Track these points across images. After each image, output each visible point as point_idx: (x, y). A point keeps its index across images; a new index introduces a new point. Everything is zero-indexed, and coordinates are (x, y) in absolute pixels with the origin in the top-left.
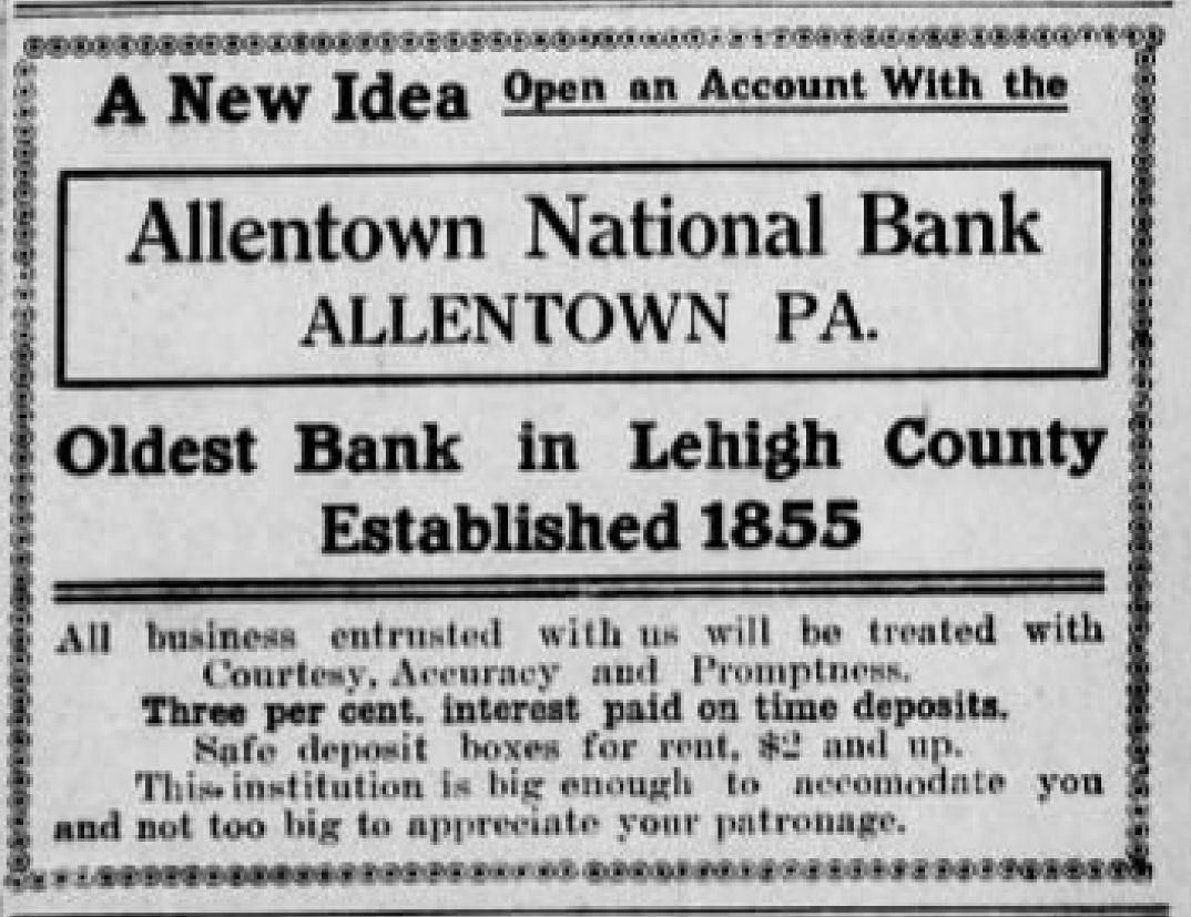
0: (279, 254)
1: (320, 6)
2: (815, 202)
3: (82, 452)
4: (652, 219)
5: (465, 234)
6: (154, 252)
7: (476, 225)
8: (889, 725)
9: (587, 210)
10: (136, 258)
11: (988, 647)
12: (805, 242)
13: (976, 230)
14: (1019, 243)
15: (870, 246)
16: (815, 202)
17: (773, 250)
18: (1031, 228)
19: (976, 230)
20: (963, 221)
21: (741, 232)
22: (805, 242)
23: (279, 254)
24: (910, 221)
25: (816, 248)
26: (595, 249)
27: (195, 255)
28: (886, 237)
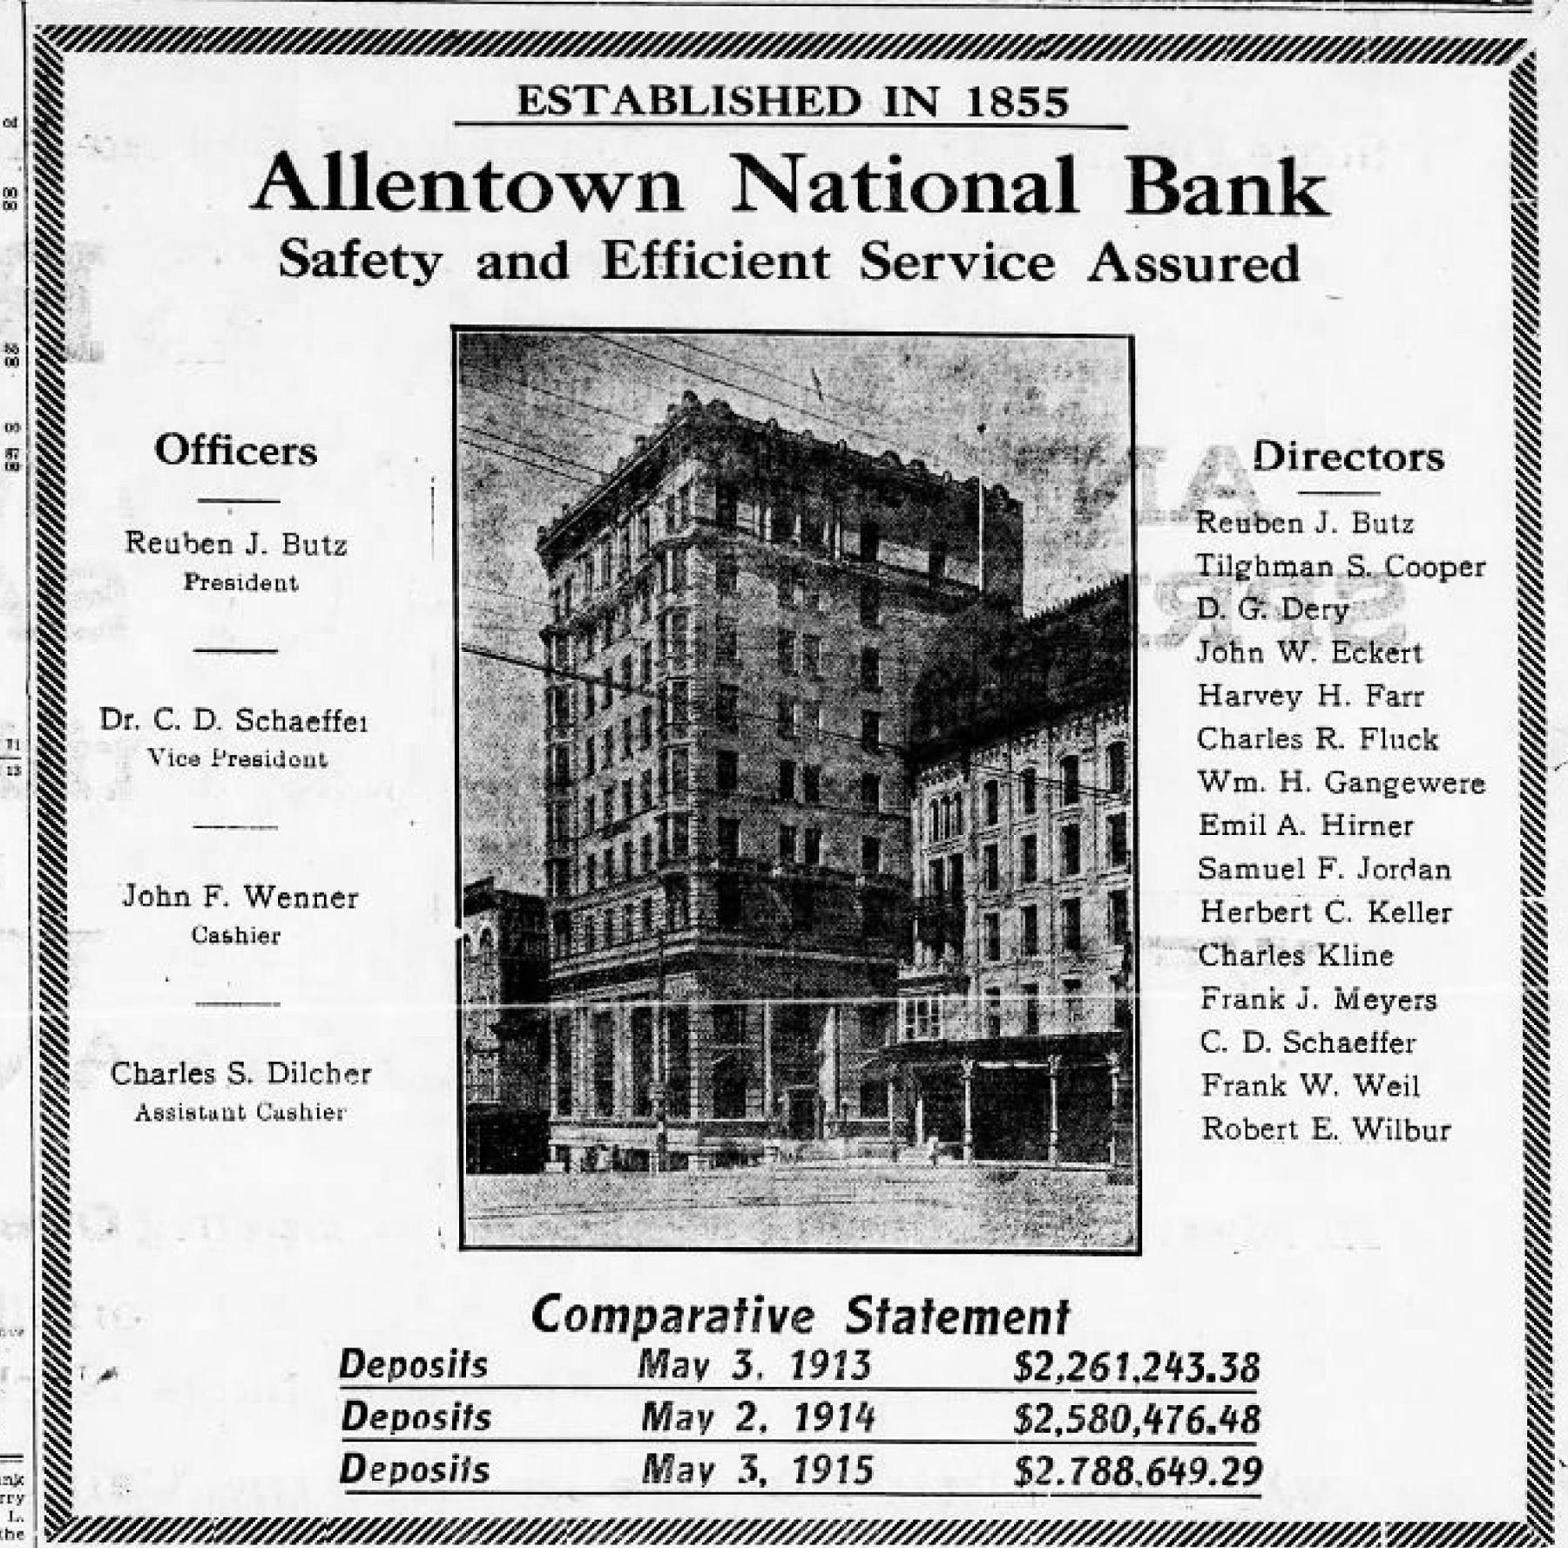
0: (430, 204)
1: (1431, 6)
2: (1067, 163)
3: (172, 448)
4: (878, 176)
5: (660, 189)
6: (1108, 272)
7: (672, 182)
8: (1115, 972)
9: (806, 171)
10: (1094, 278)
11: (189, 570)
12: (1054, 197)
13: (1251, 193)
14: (1299, 206)
15: (1139, 206)
16: (1067, 163)
17: (1020, 206)
18: (1314, 193)
19: (1251, 193)
20: (1237, 184)
21: (985, 190)
22: (1054, 197)
23: (430, 204)
24: (1177, 183)
25: (1067, 206)
26: (816, 205)
27: (335, 203)
28: (1154, 197)
